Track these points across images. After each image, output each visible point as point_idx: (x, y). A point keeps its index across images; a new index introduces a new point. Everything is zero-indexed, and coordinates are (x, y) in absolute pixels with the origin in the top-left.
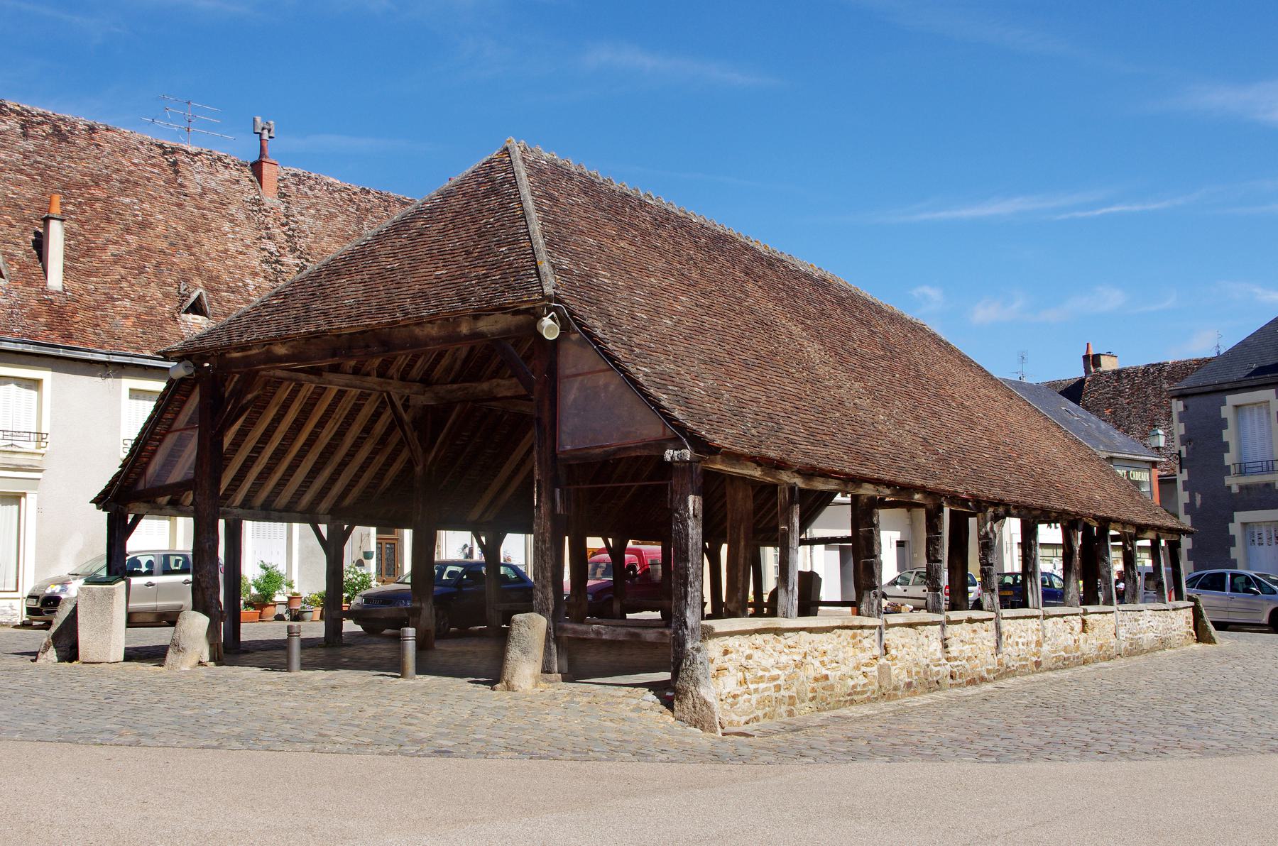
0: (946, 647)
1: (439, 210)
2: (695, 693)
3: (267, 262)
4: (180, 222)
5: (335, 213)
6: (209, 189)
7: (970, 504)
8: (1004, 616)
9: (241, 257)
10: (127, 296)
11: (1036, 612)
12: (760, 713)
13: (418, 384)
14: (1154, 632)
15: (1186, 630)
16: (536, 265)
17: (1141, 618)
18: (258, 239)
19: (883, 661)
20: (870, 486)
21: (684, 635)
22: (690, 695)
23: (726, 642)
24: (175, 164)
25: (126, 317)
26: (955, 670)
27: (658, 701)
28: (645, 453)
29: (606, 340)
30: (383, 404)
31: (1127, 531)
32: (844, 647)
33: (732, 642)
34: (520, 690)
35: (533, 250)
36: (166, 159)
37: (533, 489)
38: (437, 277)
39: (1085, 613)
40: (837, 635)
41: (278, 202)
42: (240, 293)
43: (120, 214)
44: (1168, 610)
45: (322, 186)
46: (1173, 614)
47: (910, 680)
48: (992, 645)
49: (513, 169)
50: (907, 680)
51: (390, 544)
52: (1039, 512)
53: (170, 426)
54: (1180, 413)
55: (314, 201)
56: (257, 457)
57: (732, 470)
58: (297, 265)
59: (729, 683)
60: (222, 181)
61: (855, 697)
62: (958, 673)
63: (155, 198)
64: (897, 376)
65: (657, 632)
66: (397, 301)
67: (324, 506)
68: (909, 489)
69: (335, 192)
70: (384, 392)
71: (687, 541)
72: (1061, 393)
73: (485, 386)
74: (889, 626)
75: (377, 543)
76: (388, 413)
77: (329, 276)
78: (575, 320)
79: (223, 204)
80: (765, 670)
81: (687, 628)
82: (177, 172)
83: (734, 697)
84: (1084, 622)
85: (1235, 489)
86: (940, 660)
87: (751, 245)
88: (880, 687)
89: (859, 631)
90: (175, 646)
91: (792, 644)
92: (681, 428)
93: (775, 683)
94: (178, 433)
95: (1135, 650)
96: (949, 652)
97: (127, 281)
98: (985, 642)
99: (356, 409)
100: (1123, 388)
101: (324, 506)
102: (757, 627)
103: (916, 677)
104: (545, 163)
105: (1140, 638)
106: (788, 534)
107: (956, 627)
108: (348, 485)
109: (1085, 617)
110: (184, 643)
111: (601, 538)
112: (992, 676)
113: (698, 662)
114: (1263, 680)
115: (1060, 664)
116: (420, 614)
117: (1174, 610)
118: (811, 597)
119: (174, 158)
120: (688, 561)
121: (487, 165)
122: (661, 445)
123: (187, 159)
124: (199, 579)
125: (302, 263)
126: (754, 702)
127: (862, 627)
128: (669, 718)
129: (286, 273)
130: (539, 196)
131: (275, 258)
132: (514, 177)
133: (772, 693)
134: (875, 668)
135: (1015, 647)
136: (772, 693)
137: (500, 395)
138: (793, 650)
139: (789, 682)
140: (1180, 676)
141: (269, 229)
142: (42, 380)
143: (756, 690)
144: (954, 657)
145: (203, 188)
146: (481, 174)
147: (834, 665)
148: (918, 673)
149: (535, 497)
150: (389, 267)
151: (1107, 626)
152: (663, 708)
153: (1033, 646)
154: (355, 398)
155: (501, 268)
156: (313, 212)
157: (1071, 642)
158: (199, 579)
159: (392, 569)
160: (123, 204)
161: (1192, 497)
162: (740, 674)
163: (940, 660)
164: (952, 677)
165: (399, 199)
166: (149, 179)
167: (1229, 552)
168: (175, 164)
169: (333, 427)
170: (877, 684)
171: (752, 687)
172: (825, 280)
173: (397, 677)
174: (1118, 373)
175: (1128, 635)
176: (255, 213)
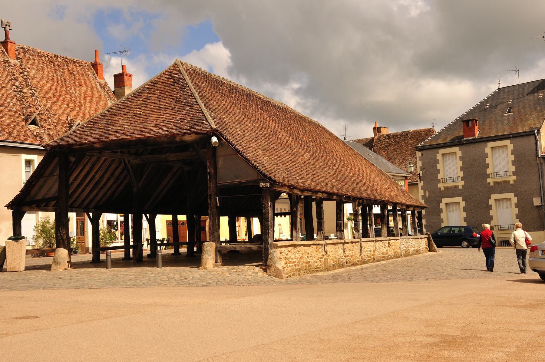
0: (344, 252)
1: (153, 89)
2: (274, 266)
3: (16, 92)
5: (44, 67)
7: (351, 199)
8: (363, 241)
9: (3, 89)
11: (373, 239)
12: (291, 274)
13: (134, 155)
14: (413, 247)
15: (425, 247)
16: (204, 115)
17: (409, 242)
18: (11, 80)
19: (325, 257)
21: (268, 247)
23: (281, 249)
26: (347, 260)
28: (251, 184)
30: (120, 163)
31: (403, 207)
33: (283, 249)
34: (209, 269)
35: (201, 109)
38: (162, 118)
39: (390, 240)
41: (16, 62)
42: (6, 107)
44: (418, 239)
46: (420, 240)
50: (333, 264)
51: (81, 221)
52: (373, 201)
54: (420, 157)
56: (71, 186)
57: (281, 190)
58: (30, 93)
61: (318, 269)
65: (258, 246)
68: (334, 194)
70: (122, 159)
71: (268, 214)
72: (363, 145)
73: (164, 156)
74: (327, 244)
75: (76, 221)
77: (111, 115)
78: (223, 137)
80: (292, 259)
81: (269, 245)
84: (389, 243)
85: (442, 189)
86: (343, 256)
88: (325, 266)
89: (318, 246)
90: (56, 262)
92: (266, 176)
95: (407, 254)
96: (345, 254)
99: (110, 165)
100: (391, 142)
101: (92, 205)
102: (289, 244)
103: (336, 263)
105: (409, 250)
106: (296, 212)
107: (347, 245)
109: (389, 241)
112: (359, 263)
114: (456, 262)
115: (381, 259)
117: (421, 239)
120: (269, 222)
121: (169, 71)
122: (258, 181)
124: (62, 236)
125: (33, 92)
126: (289, 270)
127: (319, 244)
128: (265, 275)
129: (26, 96)
132: (183, 77)
134: (323, 259)
135: (366, 252)
137: (170, 160)
138: (299, 252)
140: (426, 262)
141: (15, 75)
142: (34, 160)
143: (290, 266)
146: (167, 75)
147: (311, 258)
148: (336, 261)
149: (209, 201)
151: (397, 245)
153: (372, 252)
154: (110, 162)
156: (33, 66)
157: (385, 251)
158: (62, 236)
159: (83, 233)
161: (425, 193)
163: (343, 256)
164: (346, 263)
165: (72, 60)
167: (440, 215)
169: (101, 173)
170: (324, 265)
172: (285, 109)
174: (389, 136)
175: (405, 249)
176: (7, 67)
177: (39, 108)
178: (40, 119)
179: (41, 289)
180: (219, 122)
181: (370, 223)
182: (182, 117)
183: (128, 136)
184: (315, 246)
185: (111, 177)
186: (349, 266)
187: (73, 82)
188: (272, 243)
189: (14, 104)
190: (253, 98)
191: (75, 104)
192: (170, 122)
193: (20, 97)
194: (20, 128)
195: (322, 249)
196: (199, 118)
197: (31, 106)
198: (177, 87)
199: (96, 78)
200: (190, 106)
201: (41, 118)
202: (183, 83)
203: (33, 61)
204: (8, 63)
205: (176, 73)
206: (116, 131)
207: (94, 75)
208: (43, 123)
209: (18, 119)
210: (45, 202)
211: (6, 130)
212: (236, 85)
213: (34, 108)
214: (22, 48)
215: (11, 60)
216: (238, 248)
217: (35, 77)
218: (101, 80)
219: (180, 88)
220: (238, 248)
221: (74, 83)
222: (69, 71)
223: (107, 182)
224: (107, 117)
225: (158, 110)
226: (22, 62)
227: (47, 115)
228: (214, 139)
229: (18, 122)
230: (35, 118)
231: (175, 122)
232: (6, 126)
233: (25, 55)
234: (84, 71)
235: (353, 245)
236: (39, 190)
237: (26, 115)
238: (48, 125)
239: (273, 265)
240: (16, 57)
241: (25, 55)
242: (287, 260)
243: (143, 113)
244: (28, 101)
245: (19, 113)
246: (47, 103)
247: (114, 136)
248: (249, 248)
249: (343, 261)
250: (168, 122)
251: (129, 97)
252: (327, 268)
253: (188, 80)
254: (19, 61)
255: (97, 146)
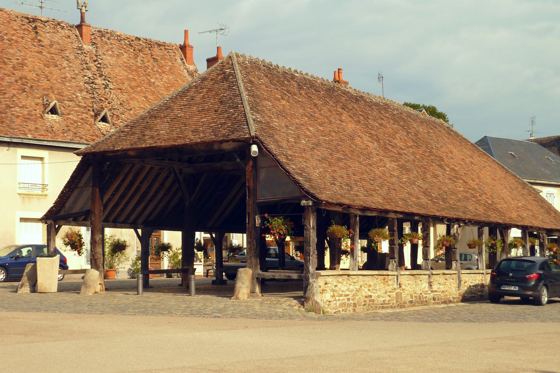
1: (200, 87)
2: (313, 299)
4: (41, 62)
6: (54, 42)
9: (73, 81)
10: (17, 105)
11: (481, 271)
16: (247, 120)
18: (82, 70)
20: (393, 214)
21: (308, 276)
22: (311, 300)
24: (35, 28)
25: (18, 117)
26: (435, 296)
27: (298, 303)
29: (277, 155)
30: (170, 172)
32: (379, 283)
33: (329, 279)
35: (245, 112)
36: (31, 25)
37: (246, 216)
38: (203, 122)
40: (376, 278)
41: (91, 48)
43: (10, 59)
45: (115, 37)
47: (411, 300)
48: (456, 286)
49: (234, 68)
50: (410, 300)
53: (77, 185)
55: (110, 46)
58: (103, 84)
59: (328, 296)
60: (61, 37)
62: (437, 298)
63: (27, 49)
64: (418, 157)
66: (185, 133)
67: (141, 220)
69: (121, 40)
73: (219, 165)
76: (173, 175)
77: (151, 118)
78: (264, 146)
79: (62, 51)
80: (343, 291)
81: (310, 273)
82: (37, 33)
83: (330, 302)
87: (347, 90)
91: (355, 281)
92: (308, 193)
93: (347, 297)
94: (80, 188)
97: (16, 97)
98: (452, 284)
99: (158, 175)
101: (141, 220)
104: (247, 62)
108: (152, 211)
110: (89, 283)
111: (133, 230)
112: (455, 300)
113: (314, 287)
116: (188, 271)
118: (385, 266)
119: (35, 25)
121: (221, 65)
123: (42, 25)
125: (106, 83)
126: (338, 304)
129: (98, 89)
130: (246, 83)
131: (92, 81)
132: (234, 72)
133: (346, 301)
134: (394, 293)
136: (346, 301)
138: (356, 284)
139: (354, 297)
141: (87, 64)
143: (339, 300)
144: (435, 291)
145: (51, 42)
147: (374, 291)
148: (416, 297)
150: (179, 115)
152: (300, 305)
155: (231, 120)
156: (110, 52)
160: (11, 53)
162: (332, 293)
163: (427, 291)
164: (434, 300)
165: (157, 43)
166: (22, 38)
168: (35, 28)
170: (395, 300)
171: (337, 298)
173: (188, 296)
176: (79, 55)
177: (111, 102)
178: (112, 115)
179: (43, 311)
180: (267, 127)
181: (480, 251)
182: (224, 121)
183: (163, 143)
184: (382, 277)
185: (160, 188)
186: (438, 303)
187: (156, 69)
188: (314, 271)
189: (84, 98)
190: (336, 94)
191: (155, 96)
192: (209, 127)
193: (91, 89)
194: (88, 126)
195: (394, 282)
196: (240, 123)
197: (103, 100)
198: (226, 84)
199: (184, 63)
200: (234, 108)
201: (114, 114)
202: (233, 80)
203: (110, 46)
204: (82, 50)
205: (228, 67)
206: (152, 137)
207: (182, 59)
208: (115, 119)
209: (86, 116)
210: (83, 215)
211: (72, 129)
212: (314, 78)
213: (105, 102)
214: (99, 31)
215: (85, 47)
216: (277, 276)
217: (110, 65)
218: (190, 66)
219: (229, 86)
220: (277, 276)
221: (157, 71)
222: (152, 55)
223: (157, 194)
224: (146, 120)
225: (200, 113)
226: (97, 48)
227: (120, 110)
228: (254, 148)
229: (86, 119)
230: (106, 114)
231: (215, 126)
232: (72, 124)
233: (102, 39)
234: (170, 55)
235: (447, 278)
236: (75, 202)
237: (96, 111)
238: (121, 122)
239: (312, 297)
240: (91, 42)
241: (102, 39)
242: (335, 293)
243: (184, 116)
244: (100, 93)
245: (89, 108)
246: (122, 96)
247: (149, 143)
248: (289, 276)
249: (428, 298)
250: (207, 127)
251: (173, 96)
252: (400, 305)
253: (239, 76)
254: (94, 47)
255: (132, 153)
